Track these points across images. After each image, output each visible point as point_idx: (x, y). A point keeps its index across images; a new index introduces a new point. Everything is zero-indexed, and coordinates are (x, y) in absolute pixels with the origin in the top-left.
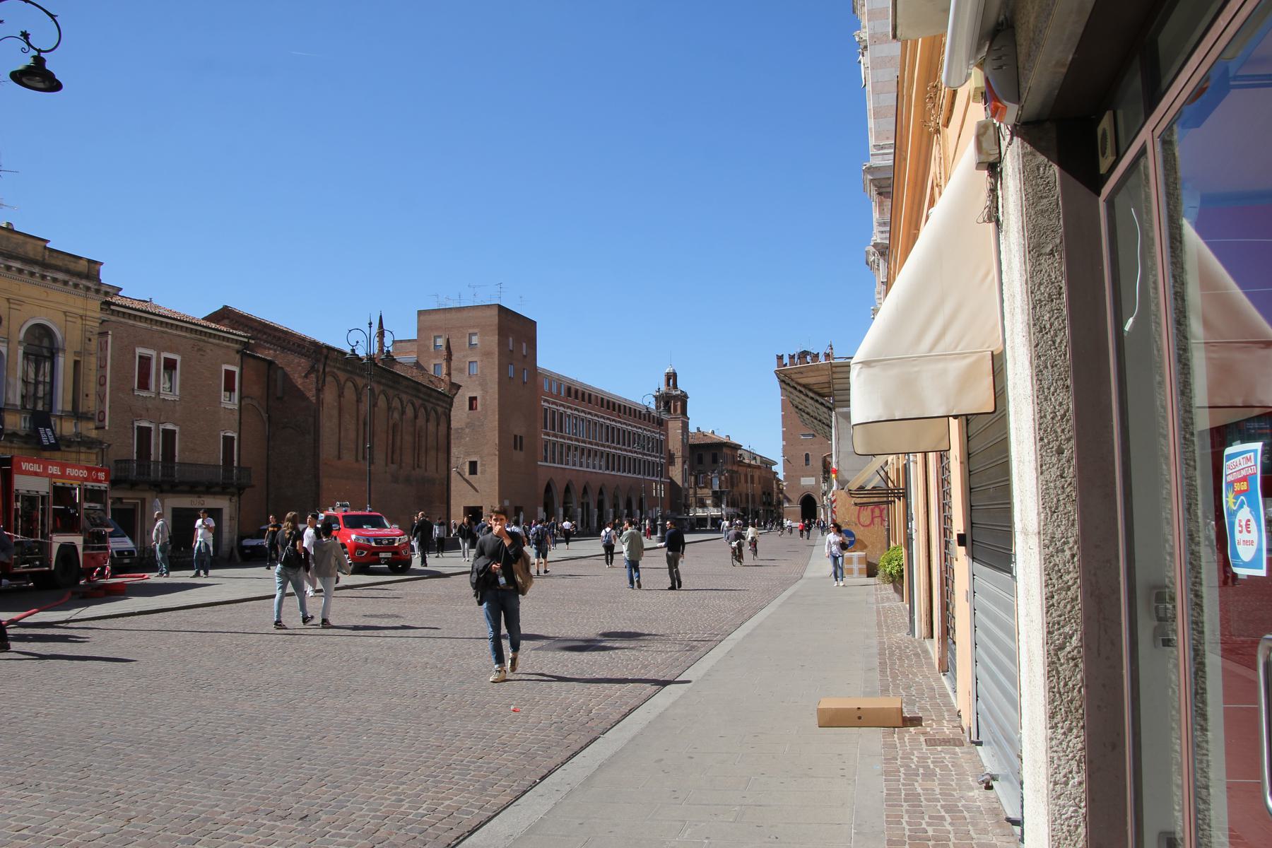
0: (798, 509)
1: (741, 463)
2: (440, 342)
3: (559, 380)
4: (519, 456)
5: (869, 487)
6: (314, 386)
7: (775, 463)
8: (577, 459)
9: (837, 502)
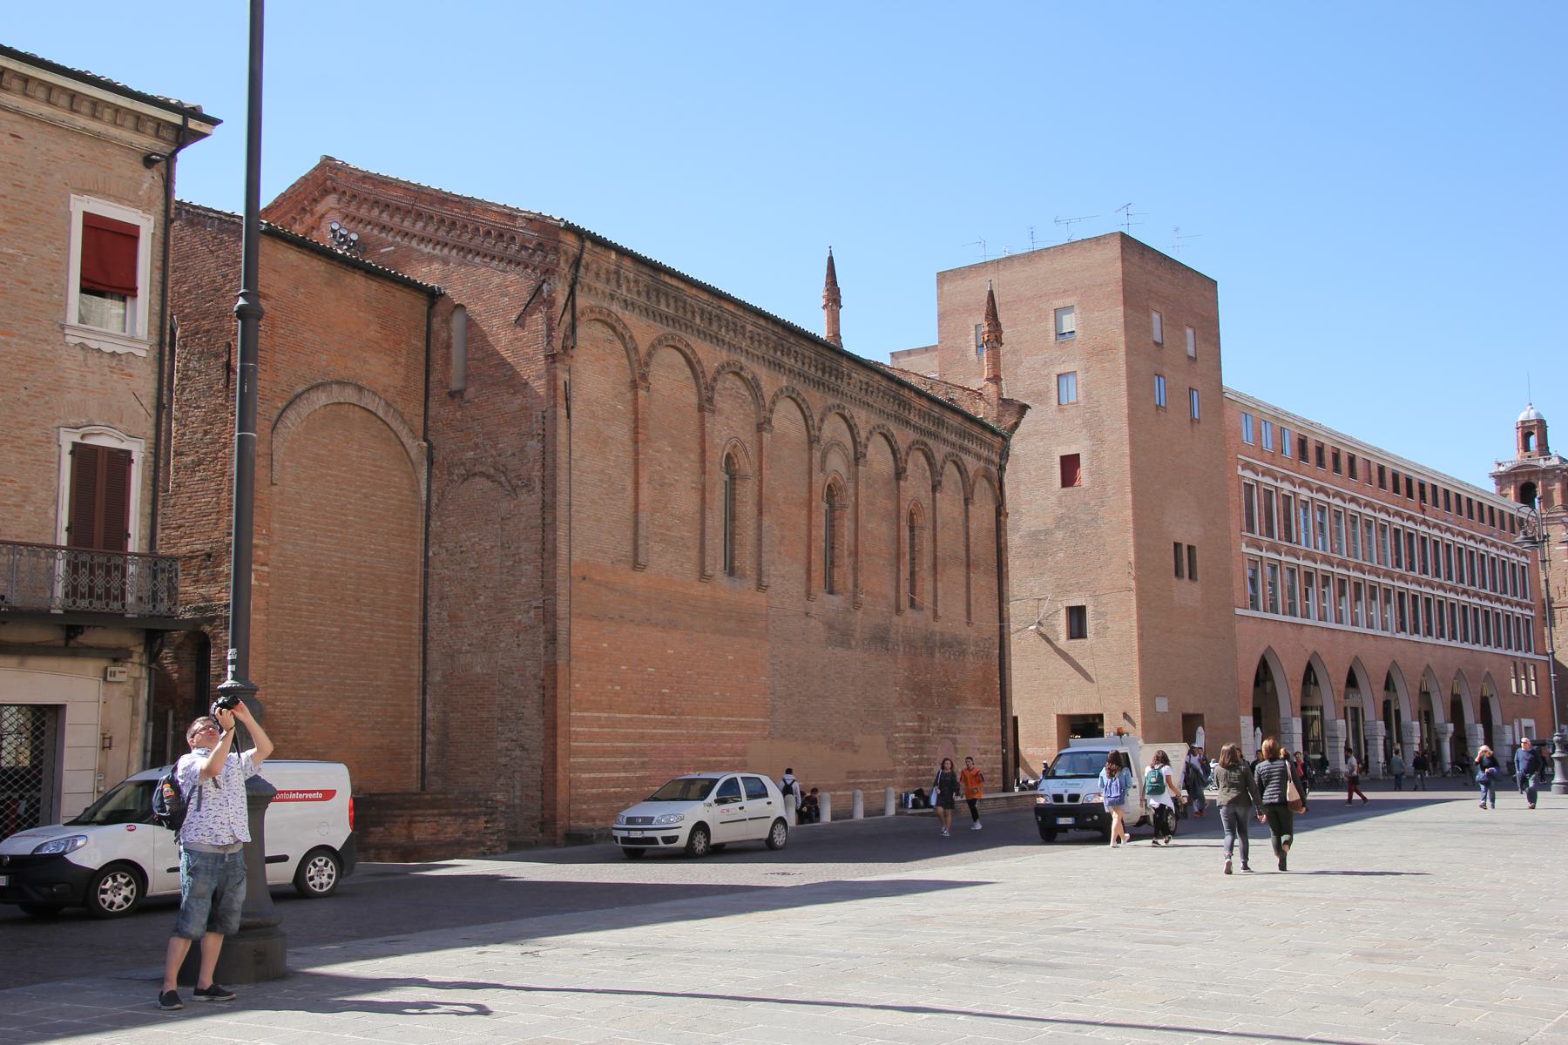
3: (1278, 421)
4: (1187, 593)
6: (542, 342)
8: (1329, 605)
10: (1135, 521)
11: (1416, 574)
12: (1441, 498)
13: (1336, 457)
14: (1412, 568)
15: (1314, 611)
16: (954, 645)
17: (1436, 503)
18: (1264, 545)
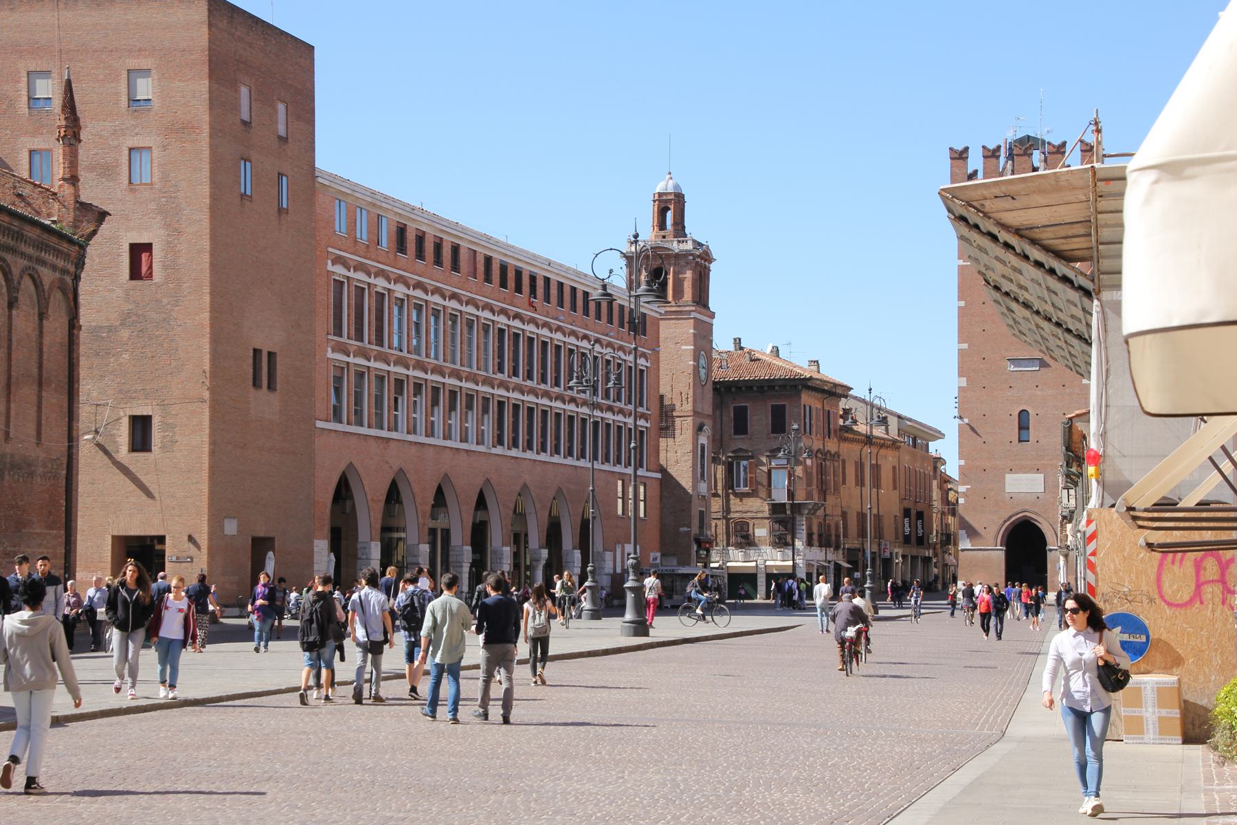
0: (998, 556)
1: (846, 434)
2: (48, 89)
4: (265, 404)
5: (1190, 501)
7: (937, 435)
8: (420, 416)
9: (1100, 548)
10: (212, 326)
11: (517, 381)
12: (554, 291)
13: (438, 247)
14: (515, 374)
15: (403, 424)
16: (23, 467)
17: (547, 299)
18: (352, 349)
